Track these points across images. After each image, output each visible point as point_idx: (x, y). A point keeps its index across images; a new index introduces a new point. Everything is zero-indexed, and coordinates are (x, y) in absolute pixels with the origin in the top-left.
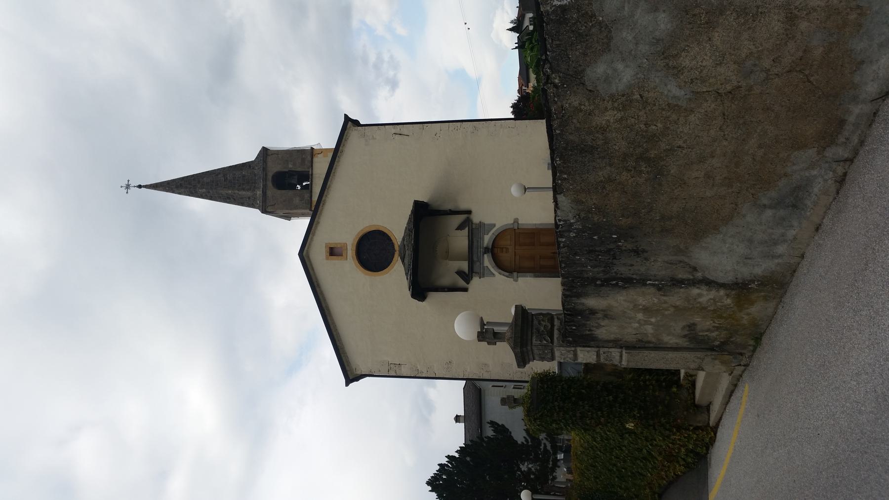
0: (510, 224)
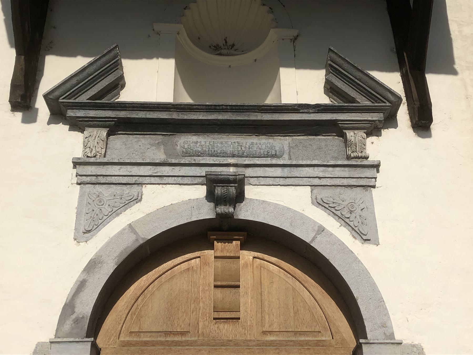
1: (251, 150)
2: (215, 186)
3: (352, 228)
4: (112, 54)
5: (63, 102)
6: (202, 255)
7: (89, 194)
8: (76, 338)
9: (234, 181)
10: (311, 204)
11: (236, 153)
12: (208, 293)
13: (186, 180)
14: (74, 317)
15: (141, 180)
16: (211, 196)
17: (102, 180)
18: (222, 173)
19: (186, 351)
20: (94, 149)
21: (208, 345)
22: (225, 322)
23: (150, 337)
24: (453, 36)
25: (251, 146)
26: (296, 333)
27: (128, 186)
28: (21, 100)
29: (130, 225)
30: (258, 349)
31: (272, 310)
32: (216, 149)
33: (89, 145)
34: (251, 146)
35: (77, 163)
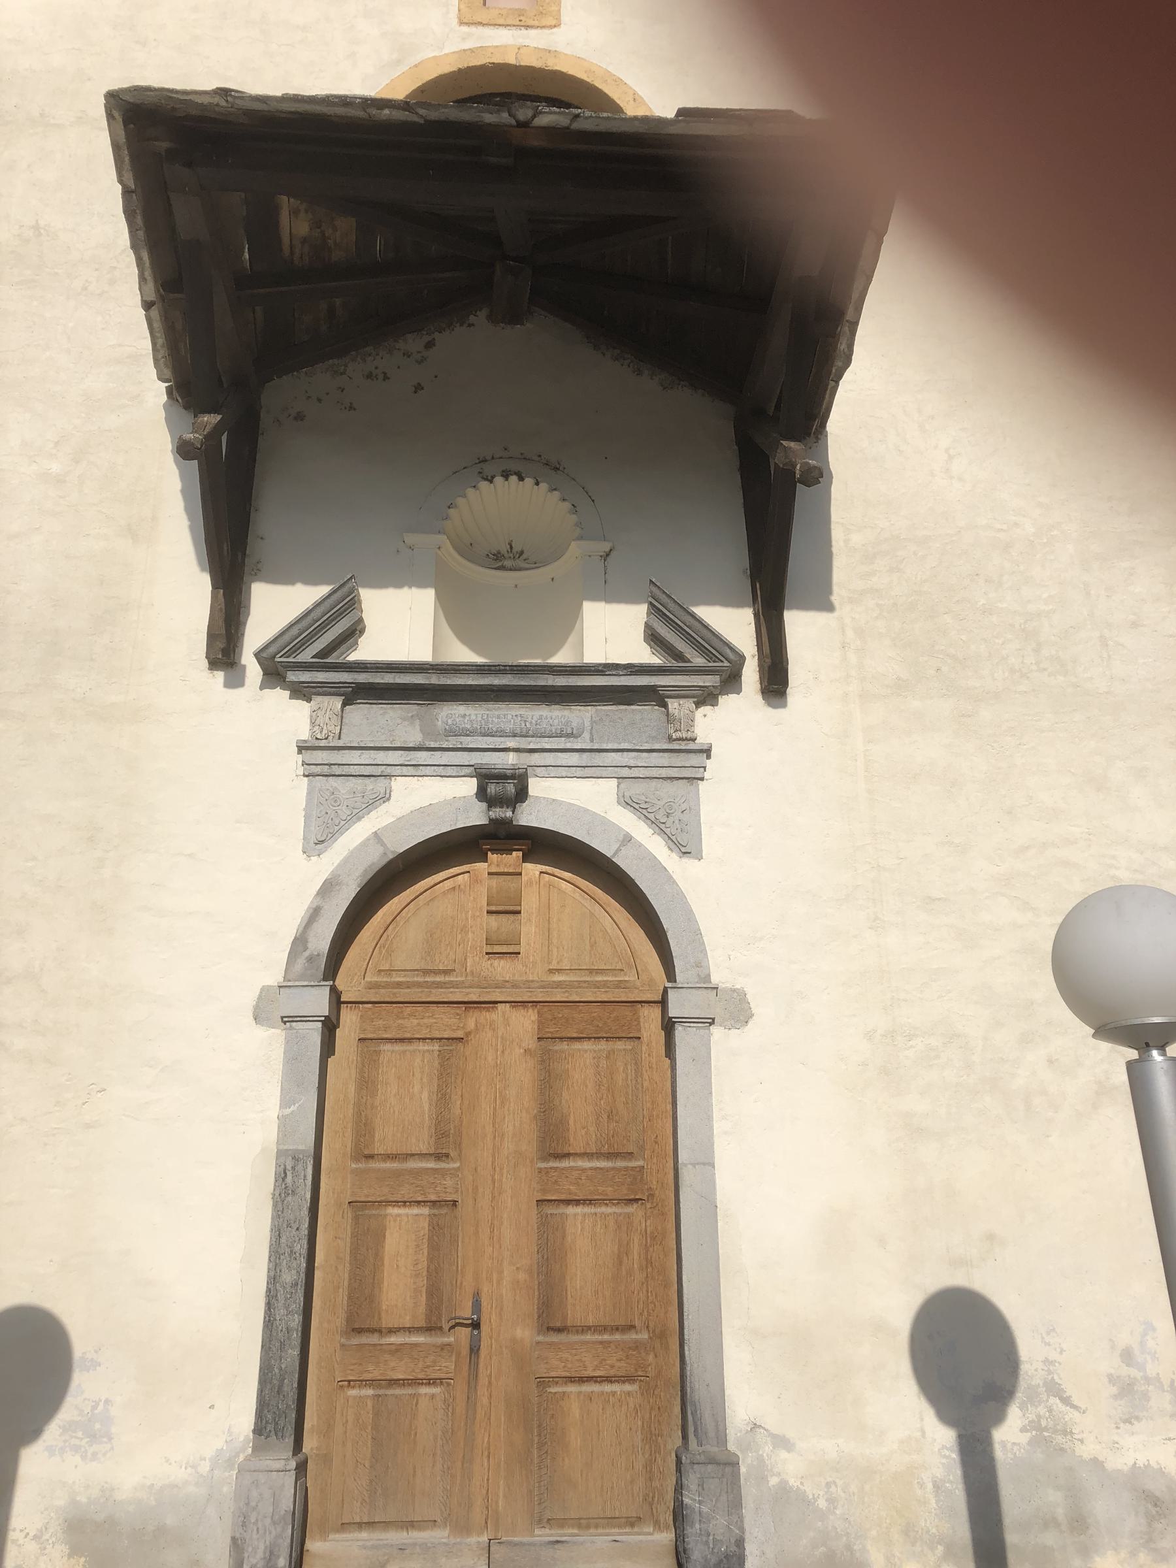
0: (700, 964)
1: (538, 726)
2: (487, 783)
3: (669, 837)
4: (346, 589)
5: (281, 662)
6: (472, 868)
7: (320, 790)
8: (311, 981)
9: (513, 777)
10: (617, 804)
11: (518, 731)
12: (479, 919)
13: (450, 771)
14: (307, 954)
15: (389, 770)
16: (482, 794)
17: (337, 770)
18: (497, 767)
19: (451, 995)
20: (325, 728)
21: (479, 987)
22: (502, 958)
23: (405, 976)
24: (834, 550)
25: (539, 721)
26: (591, 971)
27: (372, 779)
28: (223, 656)
29: (376, 833)
30: (541, 992)
31: (561, 942)
32: (490, 726)
33: (317, 722)
34: (539, 721)
35: (301, 749)
